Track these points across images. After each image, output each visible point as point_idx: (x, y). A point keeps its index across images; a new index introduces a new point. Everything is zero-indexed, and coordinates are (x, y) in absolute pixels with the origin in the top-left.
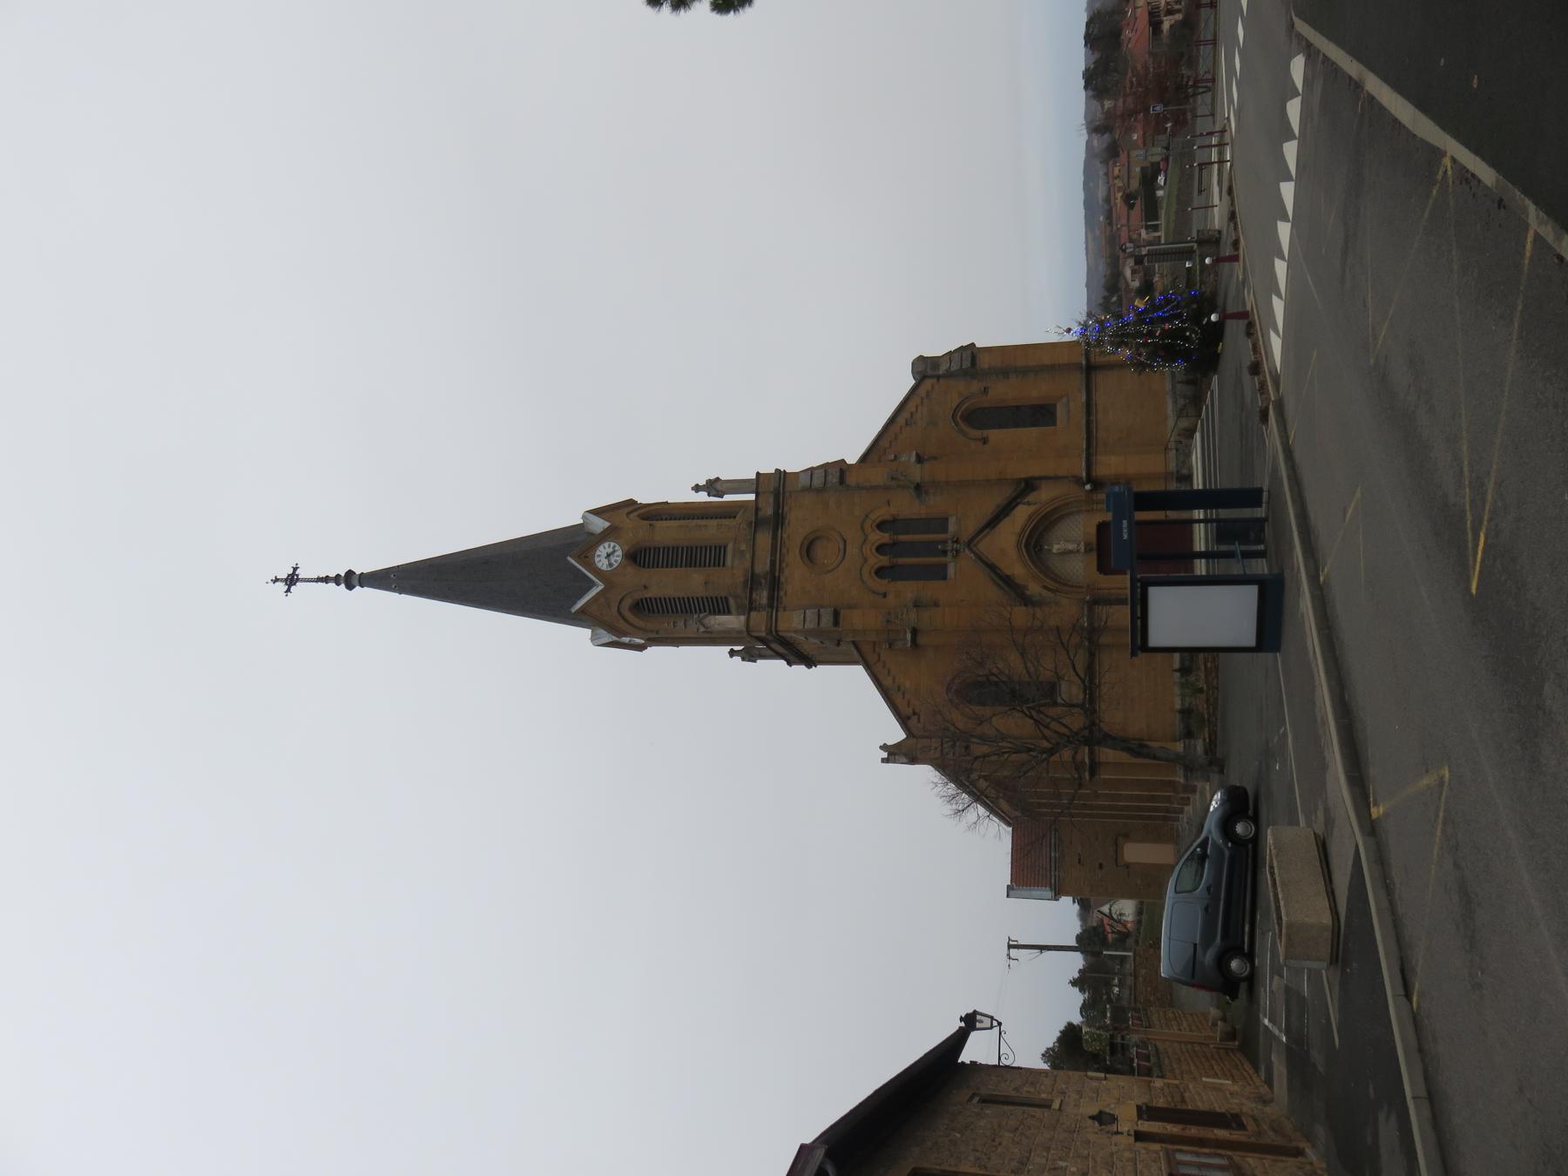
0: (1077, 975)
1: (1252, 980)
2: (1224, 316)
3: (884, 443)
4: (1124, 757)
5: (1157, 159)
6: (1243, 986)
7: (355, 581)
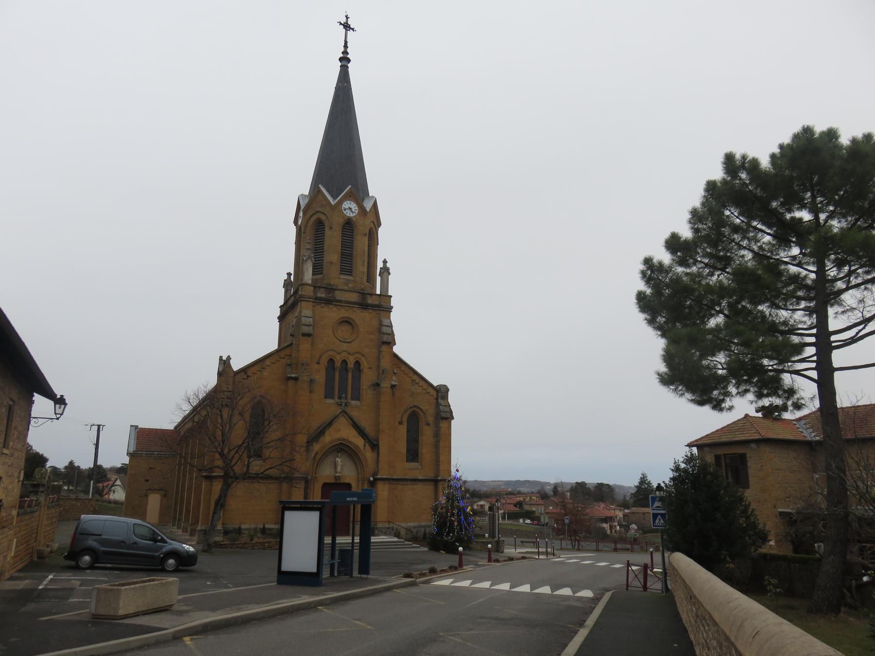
0: (76, 465)
1: (77, 568)
2: (461, 555)
3: (403, 368)
4: (215, 495)
5: (542, 519)
6: (73, 563)
7: (344, 63)
